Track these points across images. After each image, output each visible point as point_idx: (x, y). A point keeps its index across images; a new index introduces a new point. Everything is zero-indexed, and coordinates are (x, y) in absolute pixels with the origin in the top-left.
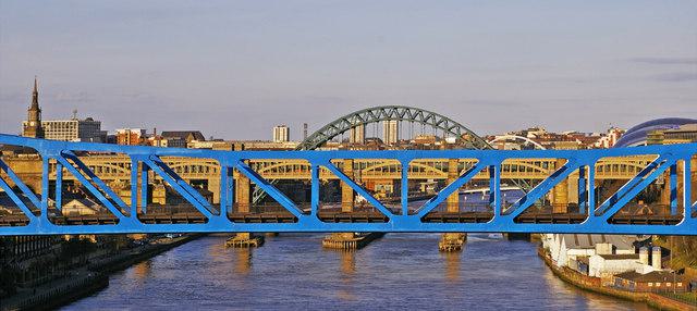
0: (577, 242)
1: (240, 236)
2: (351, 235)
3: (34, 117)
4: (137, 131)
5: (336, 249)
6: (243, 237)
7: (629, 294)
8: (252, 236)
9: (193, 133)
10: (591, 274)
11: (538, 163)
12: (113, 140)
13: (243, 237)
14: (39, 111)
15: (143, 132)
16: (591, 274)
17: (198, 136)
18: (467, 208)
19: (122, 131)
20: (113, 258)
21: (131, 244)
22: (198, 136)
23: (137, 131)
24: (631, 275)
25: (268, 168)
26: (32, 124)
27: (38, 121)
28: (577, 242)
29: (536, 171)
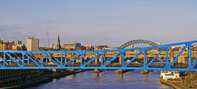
0: (163, 72)
1: (95, 70)
2: (121, 70)
3: (58, 43)
4: (90, 46)
5: (117, 73)
6: (96, 70)
7: (169, 84)
8: (98, 70)
9: (105, 46)
10: (163, 79)
11: (91, 54)
12: (85, 48)
13: (96, 70)
14: (59, 41)
15: (92, 46)
16: (163, 79)
17: (106, 47)
18: (134, 64)
19: (87, 46)
20: (48, 76)
21: (51, 72)
22: (106, 47)
23: (90, 46)
24: (171, 79)
25: (152, 54)
26: (58, 44)
27: (59, 43)
28: (163, 72)
29: (193, 55)
